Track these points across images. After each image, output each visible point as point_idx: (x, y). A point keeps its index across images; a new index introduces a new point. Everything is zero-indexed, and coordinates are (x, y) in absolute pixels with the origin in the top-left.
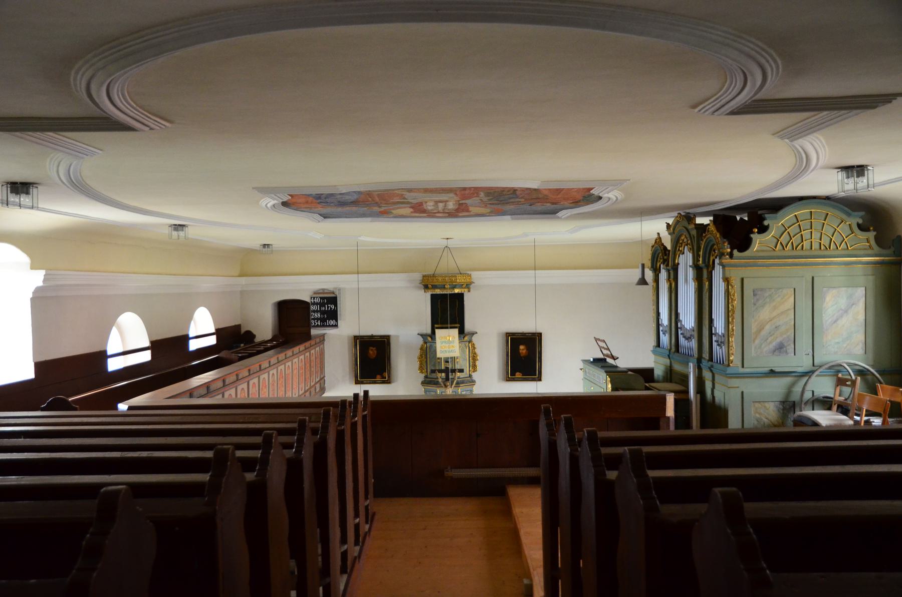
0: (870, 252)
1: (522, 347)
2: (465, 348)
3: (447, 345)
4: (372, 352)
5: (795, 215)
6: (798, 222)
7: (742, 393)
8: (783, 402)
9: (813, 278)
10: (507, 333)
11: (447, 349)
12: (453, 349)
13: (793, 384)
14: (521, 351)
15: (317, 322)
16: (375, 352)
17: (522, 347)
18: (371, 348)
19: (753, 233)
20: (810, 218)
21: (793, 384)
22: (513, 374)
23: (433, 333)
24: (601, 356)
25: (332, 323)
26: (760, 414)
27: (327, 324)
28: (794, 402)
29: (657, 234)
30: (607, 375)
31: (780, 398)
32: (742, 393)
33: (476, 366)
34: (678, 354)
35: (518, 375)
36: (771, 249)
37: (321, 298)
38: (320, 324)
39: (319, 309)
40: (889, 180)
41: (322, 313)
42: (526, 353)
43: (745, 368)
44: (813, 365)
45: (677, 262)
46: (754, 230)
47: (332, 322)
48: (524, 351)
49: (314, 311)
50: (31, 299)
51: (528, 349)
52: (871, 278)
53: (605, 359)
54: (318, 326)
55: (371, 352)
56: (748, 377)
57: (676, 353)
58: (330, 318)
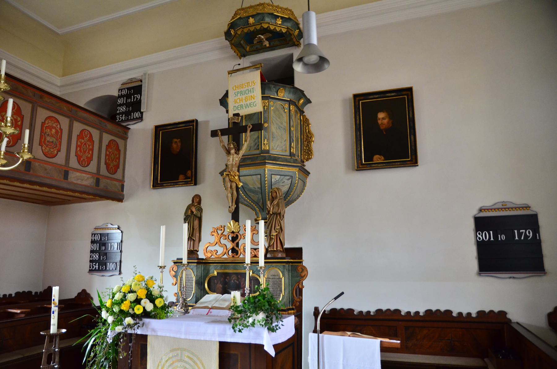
1: (381, 115)
2: (282, 111)
3: (244, 97)
4: (176, 145)
10: (355, 96)
11: (243, 103)
12: (253, 101)
14: (380, 122)
15: (122, 117)
16: (179, 144)
17: (381, 115)
18: (175, 140)
22: (369, 158)
25: (137, 115)
27: (131, 117)
35: (377, 158)
37: (128, 89)
38: (125, 119)
39: (125, 102)
41: (127, 105)
42: (388, 122)
47: (137, 115)
48: (385, 121)
49: (121, 105)
51: (391, 116)
54: (95, 270)
55: (174, 146)
58: (134, 111)
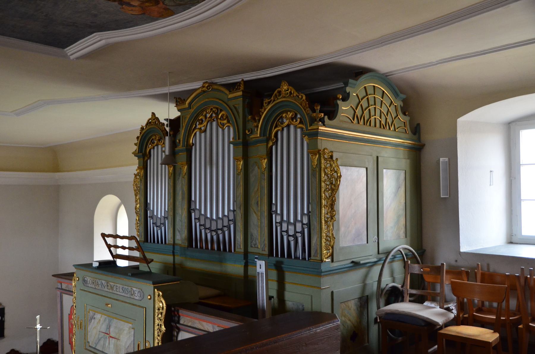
0: (403, 135)
5: (365, 87)
6: (374, 94)
7: (332, 292)
8: (360, 299)
9: (377, 157)
13: (366, 276)
19: (338, 99)
20: (373, 93)
21: (366, 276)
23: (200, 216)
24: (110, 258)
26: (345, 316)
28: (367, 296)
29: (151, 114)
30: (155, 288)
31: (357, 295)
32: (332, 292)
33: (70, 344)
34: (191, 249)
36: (350, 121)
40: (458, 56)
43: (336, 262)
44: (378, 253)
45: (191, 142)
46: (338, 96)
50: (124, 250)
52: (408, 161)
53: (114, 262)
56: (337, 273)
57: (189, 248)
